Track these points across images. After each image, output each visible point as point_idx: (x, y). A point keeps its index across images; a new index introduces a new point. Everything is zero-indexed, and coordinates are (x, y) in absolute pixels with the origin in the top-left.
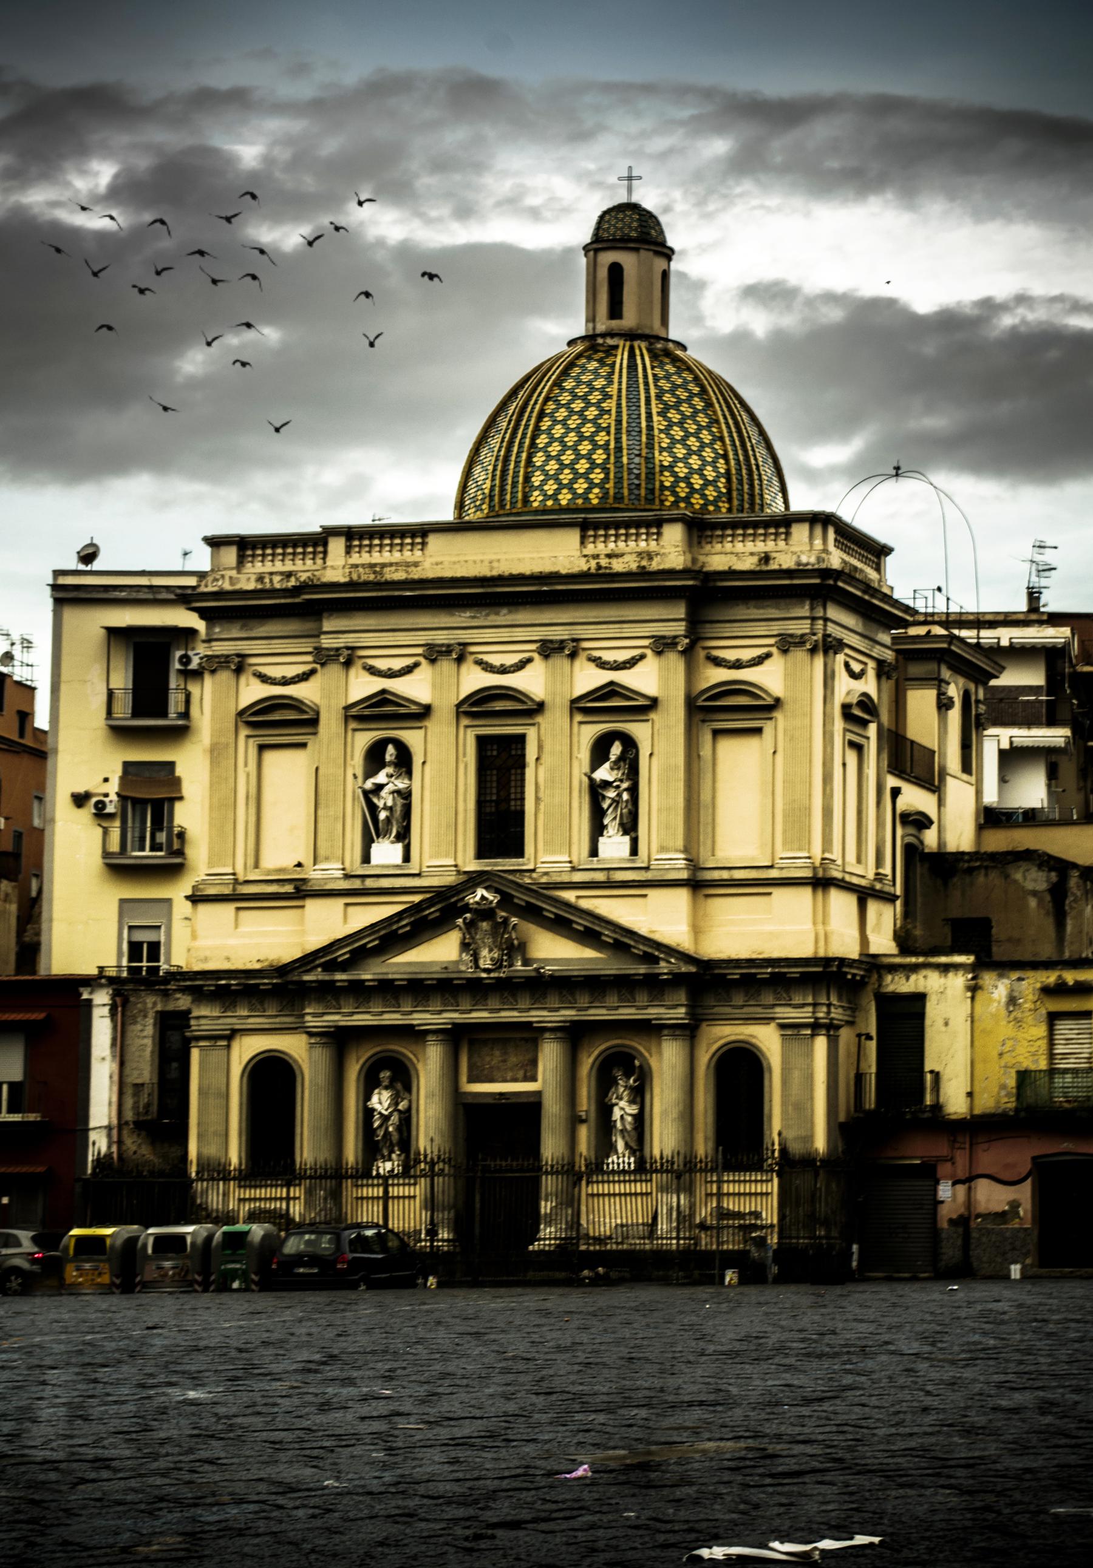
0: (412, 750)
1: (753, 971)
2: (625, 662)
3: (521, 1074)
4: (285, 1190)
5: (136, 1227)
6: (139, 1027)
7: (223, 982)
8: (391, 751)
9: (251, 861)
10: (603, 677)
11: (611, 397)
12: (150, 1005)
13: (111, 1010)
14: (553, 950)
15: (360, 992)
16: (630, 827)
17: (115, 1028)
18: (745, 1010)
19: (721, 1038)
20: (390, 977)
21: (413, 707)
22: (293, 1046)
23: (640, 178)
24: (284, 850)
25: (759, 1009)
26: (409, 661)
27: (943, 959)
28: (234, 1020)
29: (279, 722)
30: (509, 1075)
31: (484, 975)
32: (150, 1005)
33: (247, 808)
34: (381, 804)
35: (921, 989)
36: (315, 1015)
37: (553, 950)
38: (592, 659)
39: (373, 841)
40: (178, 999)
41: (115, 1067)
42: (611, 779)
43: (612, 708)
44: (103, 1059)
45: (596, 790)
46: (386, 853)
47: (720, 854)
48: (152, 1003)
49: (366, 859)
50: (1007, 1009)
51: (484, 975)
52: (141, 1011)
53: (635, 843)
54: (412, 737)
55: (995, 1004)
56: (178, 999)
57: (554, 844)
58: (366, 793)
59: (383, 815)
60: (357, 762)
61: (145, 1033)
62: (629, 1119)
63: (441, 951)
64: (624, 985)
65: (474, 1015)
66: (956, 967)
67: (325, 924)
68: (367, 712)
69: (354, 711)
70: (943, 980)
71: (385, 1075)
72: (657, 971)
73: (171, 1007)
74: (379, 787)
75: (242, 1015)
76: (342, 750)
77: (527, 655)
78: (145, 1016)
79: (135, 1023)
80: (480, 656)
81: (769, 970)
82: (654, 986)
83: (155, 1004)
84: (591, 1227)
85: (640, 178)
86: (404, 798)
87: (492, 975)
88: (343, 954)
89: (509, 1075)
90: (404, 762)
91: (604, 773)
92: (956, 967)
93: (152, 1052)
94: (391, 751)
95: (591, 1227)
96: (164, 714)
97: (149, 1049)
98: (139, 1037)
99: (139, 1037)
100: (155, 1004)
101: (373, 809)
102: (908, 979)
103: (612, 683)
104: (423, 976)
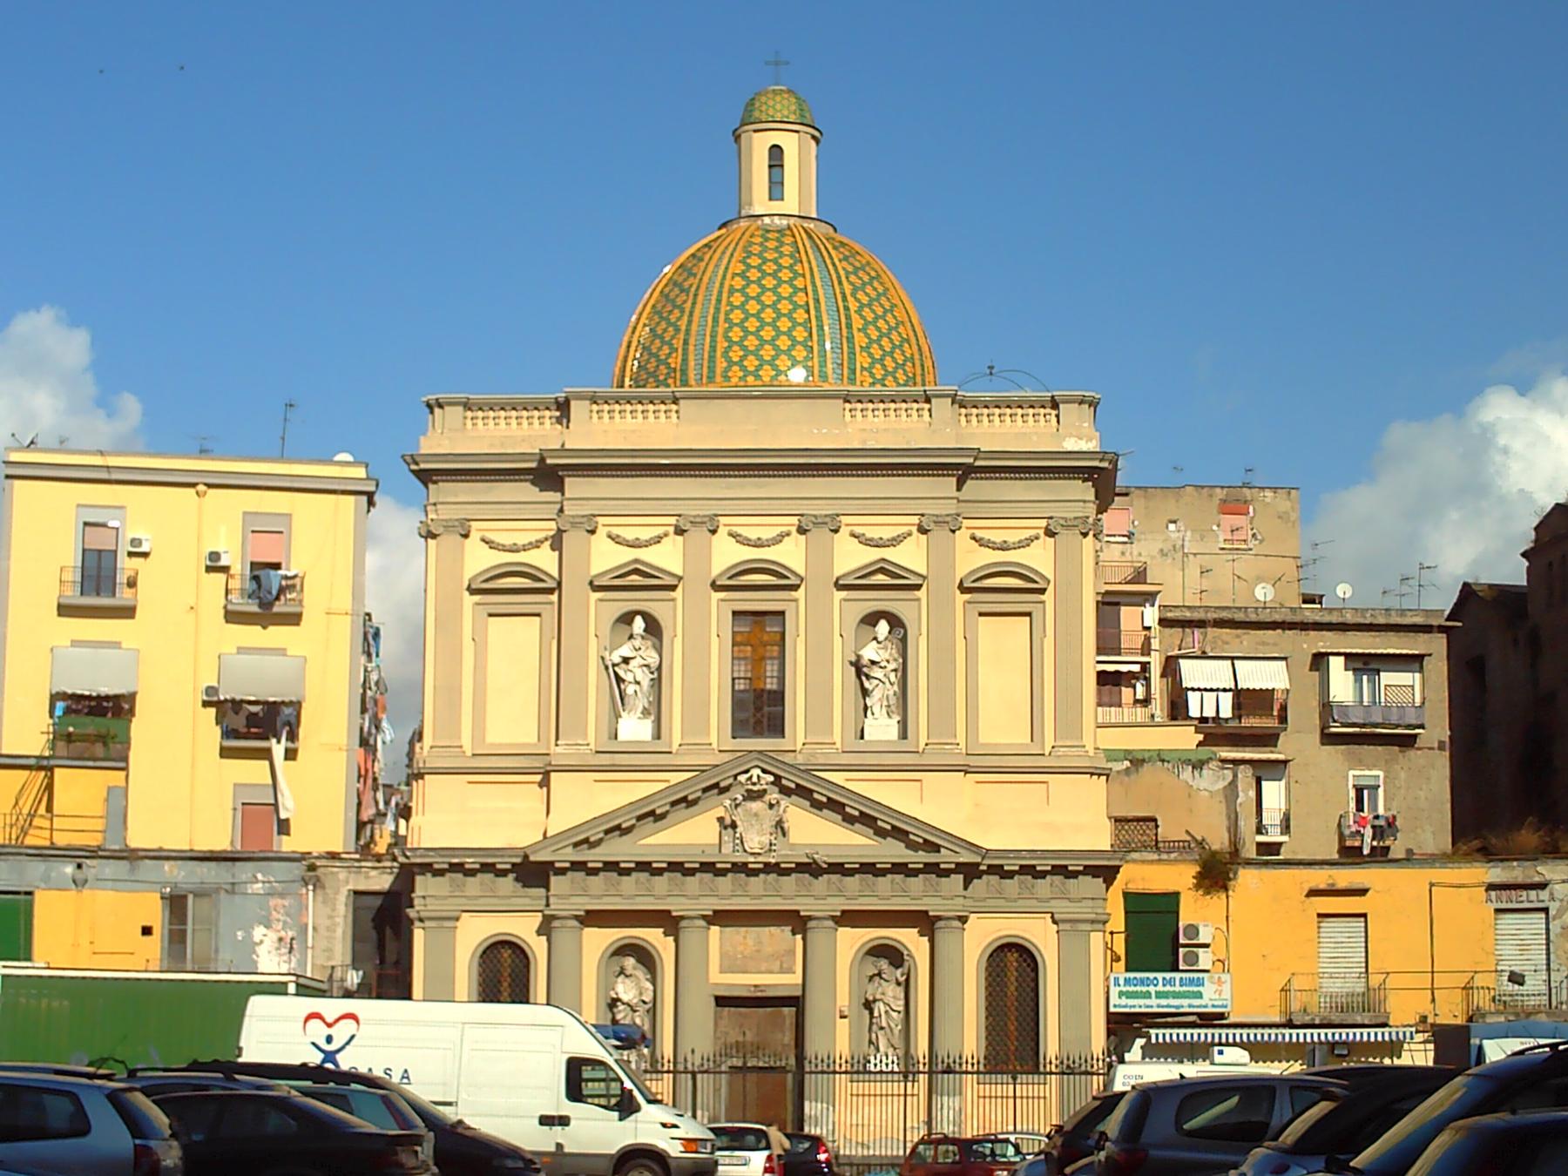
0: (663, 624)
2: (894, 539)
4: (1011, 1087)
5: (166, 1120)
10: (874, 554)
11: (695, 275)
14: (813, 833)
16: (655, 710)
18: (1020, 902)
23: (767, 63)
24: (1002, 723)
26: (659, 531)
31: (752, 859)
34: (629, 677)
37: (813, 833)
39: (618, 716)
47: (981, 740)
51: (752, 859)
53: (903, 724)
57: (815, 724)
67: (582, 801)
77: (785, 529)
80: (735, 529)
85: (767, 63)
87: (760, 859)
103: (636, 561)
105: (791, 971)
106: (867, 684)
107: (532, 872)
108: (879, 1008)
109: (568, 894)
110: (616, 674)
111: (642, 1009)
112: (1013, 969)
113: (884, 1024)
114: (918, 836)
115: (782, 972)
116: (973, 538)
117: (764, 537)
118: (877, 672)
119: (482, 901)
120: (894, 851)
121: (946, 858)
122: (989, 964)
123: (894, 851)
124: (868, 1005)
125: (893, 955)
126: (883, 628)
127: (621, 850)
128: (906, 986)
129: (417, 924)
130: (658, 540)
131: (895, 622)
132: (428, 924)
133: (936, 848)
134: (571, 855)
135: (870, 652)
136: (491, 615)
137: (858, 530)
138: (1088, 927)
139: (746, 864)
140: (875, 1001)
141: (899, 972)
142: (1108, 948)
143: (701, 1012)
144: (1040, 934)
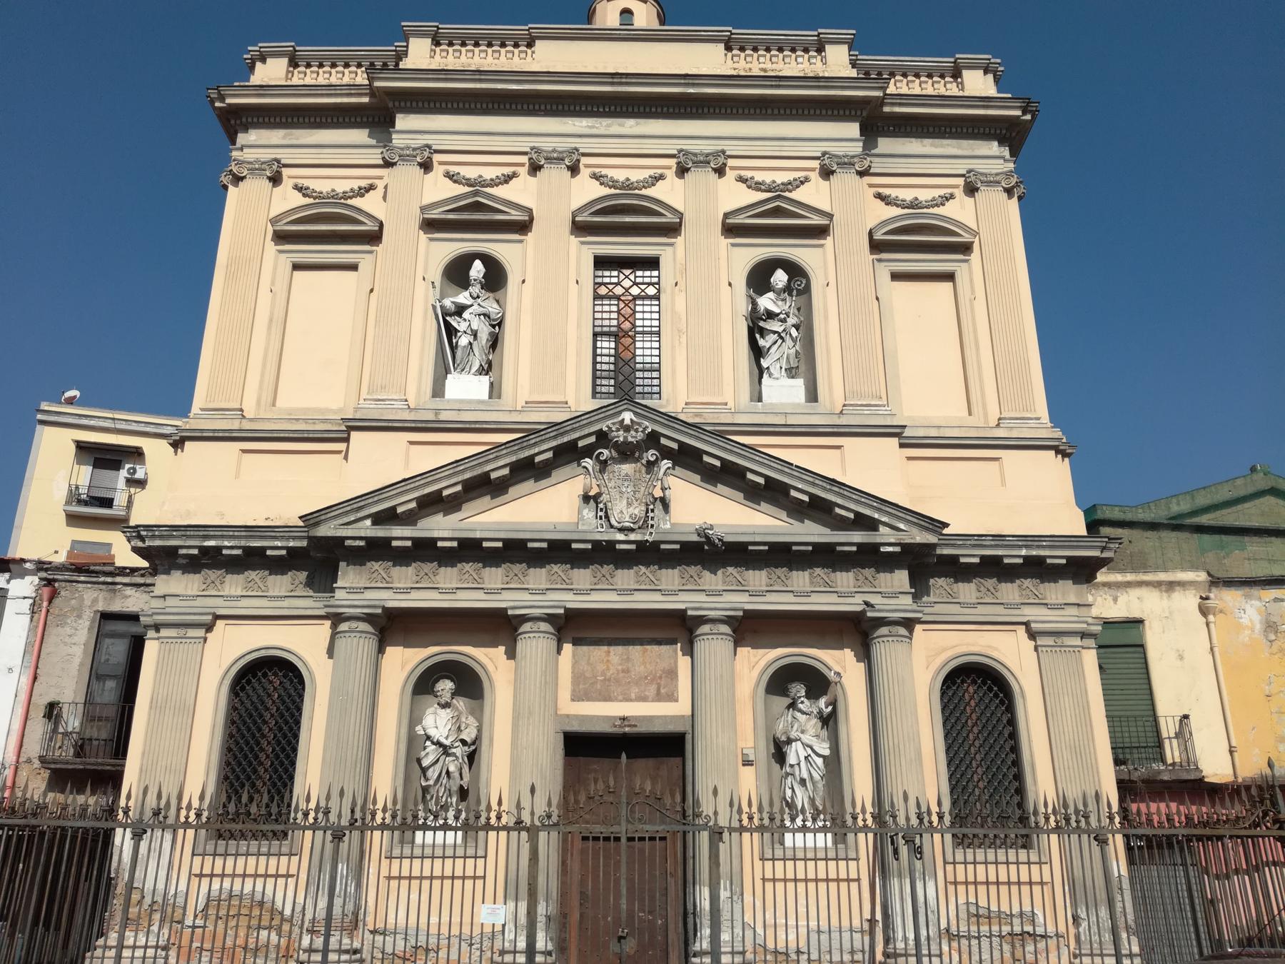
1: (1000, 552)
3: (651, 691)
6: (68, 630)
7: (212, 543)
8: (477, 269)
9: (266, 397)
12: (87, 602)
13: (33, 605)
14: (698, 508)
15: (425, 551)
17: (32, 630)
19: (944, 650)
20: (478, 535)
21: (513, 212)
22: (305, 643)
24: (929, 400)
25: (1000, 609)
27: (1162, 576)
28: (219, 602)
29: (328, 233)
30: (634, 692)
31: (620, 537)
32: (87, 602)
33: (269, 333)
35: (1136, 614)
36: (351, 590)
37: (698, 508)
38: (741, 180)
39: (447, 371)
40: (127, 597)
41: (25, 680)
42: (777, 310)
43: (776, 222)
44: (10, 670)
45: (756, 326)
46: (466, 388)
48: (92, 599)
49: (438, 391)
50: (1266, 637)
51: (620, 537)
52: (73, 609)
54: (503, 249)
55: (1247, 632)
56: (127, 597)
58: (446, 313)
59: (464, 341)
60: (436, 274)
61: (75, 639)
62: (820, 761)
63: (550, 508)
64: (824, 557)
65: (595, 596)
66: (1182, 584)
67: (381, 464)
68: (451, 216)
69: (435, 214)
70: (1165, 602)
71: (445, 686)
72: (878, 540)
73: (117, 606)
74: (460, 310)
75: (233, 589)
76: (413, 263)
78: (79, 617)
79: (62, 625)
81: (1024, 552)
82: (870, 557)
83: (95, 601)
84: (770, 932)
86: (494, 326)
87: (632, 537)
88: (405, 503)
89: (634, 692)
90: (495, 278)
91: (766, 302)
92: (1182, 584)
93: (81, 664)
94: (477, 269)
95: (770, 932)
96: (184, 411)
97: (77, 661)
98: (65, 644)
99: (65, 644)
100: (95, 601)
101: (451, 331)
102: (1115, 600)
104: (527, 536)
105: (672, 697)
106: (761, 342)
107: (316, 556)
108: (795, 753)
109: (360, 588)
110: (446, 322)
111: (459, 751)
112: (976, 697)
113: (805, 775)
114: (847, 508)
115: (659, 697)
116: (879, 196)
117: (633, 179)
118: (775, 326)
119: (245, 602)
120: (811, 532)
121: (886, 537)
122: (943, 693)
123: (811, 532)
124: (779, 756)
125: (817, 683)
126: (780, 278)
127: (440, 527)
128: (829, 721)
129: (151, 634)
130: (507, 179)
131: (795, 270)
132: (164, 632)
133: (872, 525)
134: (367, 529)
135: (766, 302)
136: (297, 267)
137: (748, 174)
138: (1077, 641)
139: (612, 543)
140: (789, 741)
141: (822, 702)
142: (894, 817)
143: (547, 762)
144: (1011, 652)
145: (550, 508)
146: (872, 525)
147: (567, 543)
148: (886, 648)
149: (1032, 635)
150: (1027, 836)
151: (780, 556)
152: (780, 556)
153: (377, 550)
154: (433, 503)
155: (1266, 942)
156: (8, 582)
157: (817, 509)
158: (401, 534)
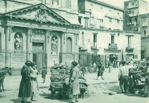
14: (50, 19)
15: (19, 20)
37: (50, 19)
63: (32, 15)
64: (60, 25)
120: (58, 22)
123: (58, 22)
145: (32, 15)
146: (64, 22)
147: (53, 23)
148: (63, 35)
149: (74, 34)
150: (41, 44)
151: (56, 25)
152: (56, 25)
153: (14, 19)
154: (20, 13)
155: (80, 67)
156: (122, 20)
157: (60, 20)
158: (17, 17)
